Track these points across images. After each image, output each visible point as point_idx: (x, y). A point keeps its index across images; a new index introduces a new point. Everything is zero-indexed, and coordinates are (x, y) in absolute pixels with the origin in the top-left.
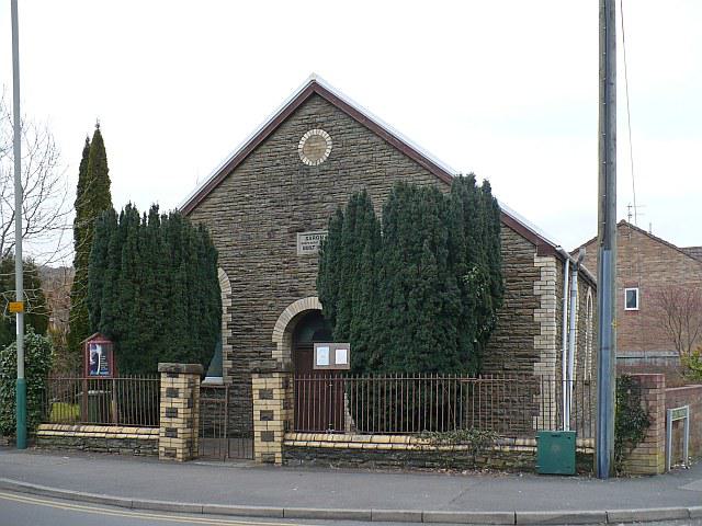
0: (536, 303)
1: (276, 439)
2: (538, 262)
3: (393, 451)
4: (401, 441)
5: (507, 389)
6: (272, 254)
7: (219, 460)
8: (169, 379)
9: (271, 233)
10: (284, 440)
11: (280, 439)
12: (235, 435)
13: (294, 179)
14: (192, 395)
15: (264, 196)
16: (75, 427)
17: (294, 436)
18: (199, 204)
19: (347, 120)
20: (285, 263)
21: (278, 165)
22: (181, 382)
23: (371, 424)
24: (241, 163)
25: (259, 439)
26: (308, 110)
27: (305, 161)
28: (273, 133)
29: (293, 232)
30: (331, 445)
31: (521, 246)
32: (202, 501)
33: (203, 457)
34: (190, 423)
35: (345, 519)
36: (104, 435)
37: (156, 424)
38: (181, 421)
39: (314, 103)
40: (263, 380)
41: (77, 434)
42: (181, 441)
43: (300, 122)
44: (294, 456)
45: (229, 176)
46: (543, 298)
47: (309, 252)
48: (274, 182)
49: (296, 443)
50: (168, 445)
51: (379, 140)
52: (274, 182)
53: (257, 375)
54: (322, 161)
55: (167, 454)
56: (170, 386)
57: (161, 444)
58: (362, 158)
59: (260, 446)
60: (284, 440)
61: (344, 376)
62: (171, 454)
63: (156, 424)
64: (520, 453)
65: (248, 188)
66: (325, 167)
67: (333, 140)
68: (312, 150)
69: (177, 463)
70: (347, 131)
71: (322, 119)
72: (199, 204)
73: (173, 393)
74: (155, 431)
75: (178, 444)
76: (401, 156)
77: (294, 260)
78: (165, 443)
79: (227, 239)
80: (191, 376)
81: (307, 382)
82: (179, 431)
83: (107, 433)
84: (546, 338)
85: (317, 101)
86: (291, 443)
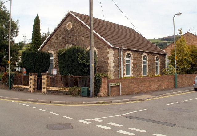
0: (108, 59)
2: (109, 50)
9: (62, 45)
10: (47, 89)
13: (66, 33)
14: (35, 79)
24: (57, 30)
29: (65, 44)
35: (78, 104)
37: (28, 85)
39: (69, 16)
44: (52, 92)
45: (55, 33)
48: (62, 34)
52: (62, 34)
58: (77, 28)
59: (43, 90)
63: (28, 85)
68: (69, 27)
73: (31, 79)
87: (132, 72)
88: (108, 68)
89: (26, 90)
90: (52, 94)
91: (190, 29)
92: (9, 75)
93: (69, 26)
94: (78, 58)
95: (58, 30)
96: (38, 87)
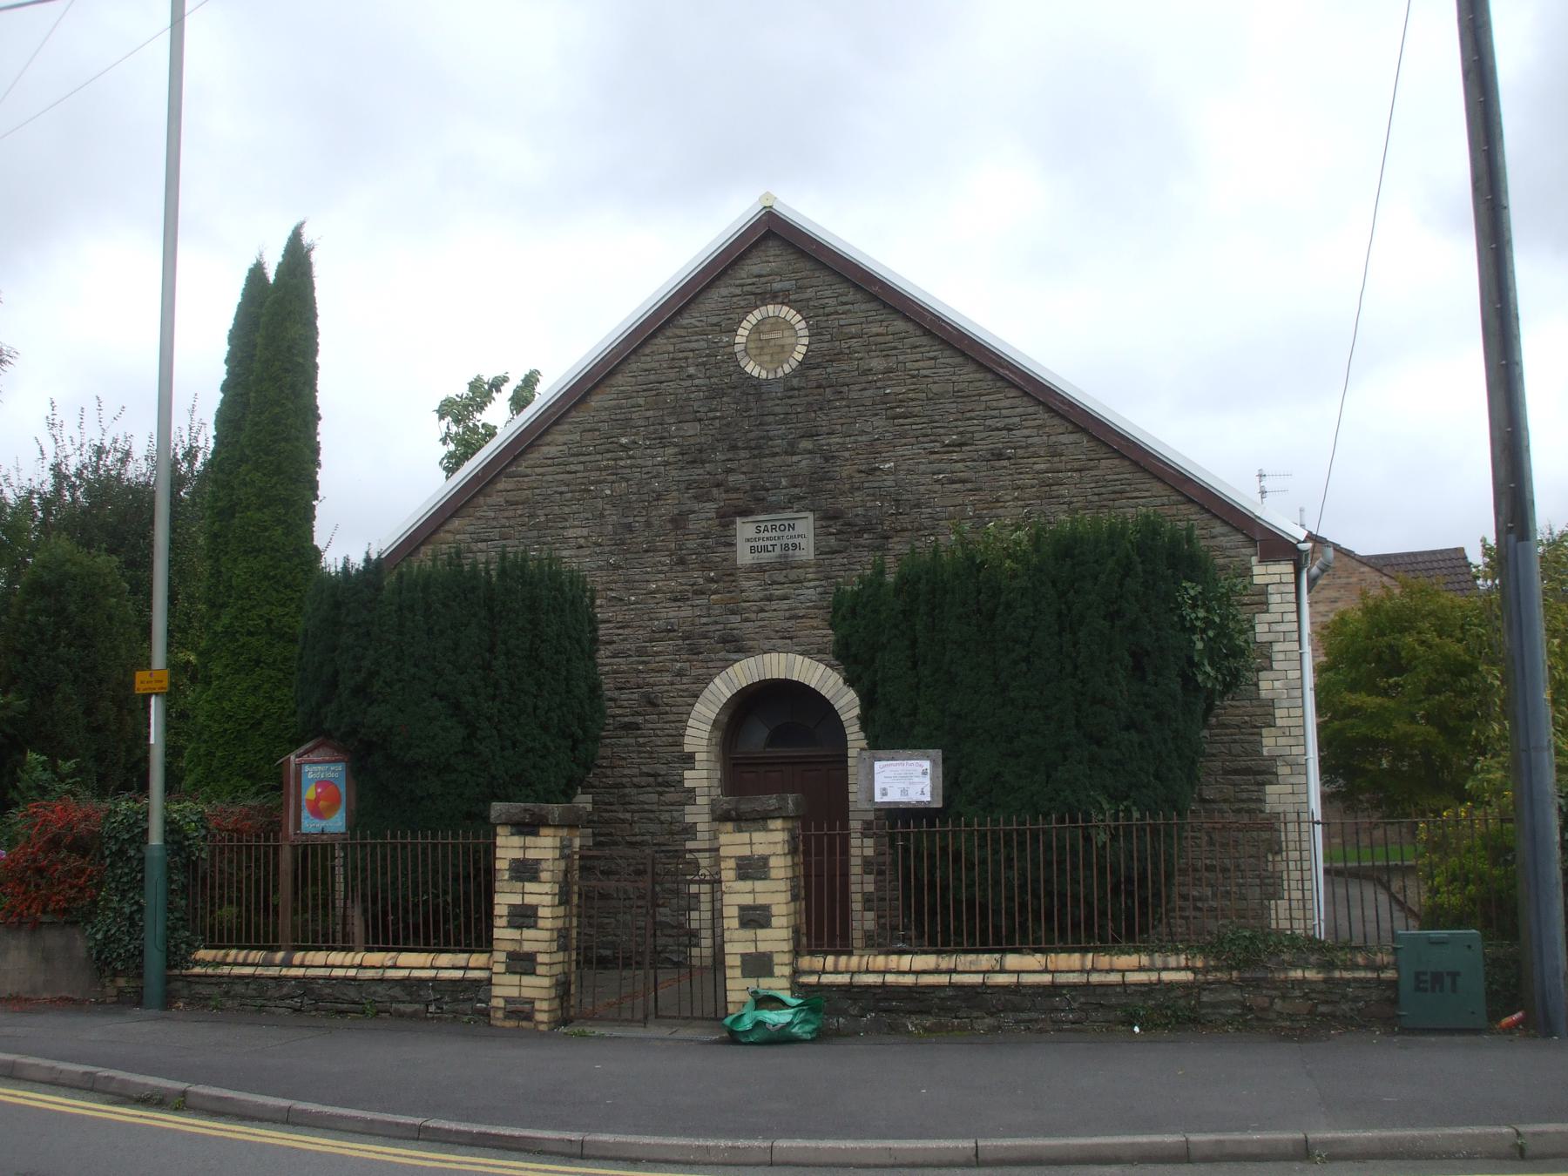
1: (777, 970)
3: (1054, 989)
4: (1069, 966)
5: (1211, 843)
6: (682, 562)
7: (631, 1021)
8: (517, 840)
11: (787, 971)
12: (603, 963)
15: (663, 442)
16: (280, 955)
17: (817, 962)
18: (516, 458)
19: (841, 288)
20: (712, 580)
21: (690, 377)
22: (544, 847)
23: (997, 928)
25: (738, 972)
26: (754, 266)
27: (752, 368)
28: (680, 312)
29: (726, 518)
30: (909, 980)
31: (1222, 541)
32: (766, 1133)
33: (593, 1018)
34: (562, 939)
36: (352, 973)
37: (484, 943)
38: (546, 935)
39: (772, 237)
40: (745, 837)
41: (285, 972)
42: (546, 982)
43: (738, 291)
44: (839, 1014)
46: (1276, 647)
47: (765, 557)
49: (826, 979)
50: (514, 992)
51: (910, 327)
53: (729, 826)
54: (787, 369)
55: (510, 1014)
56: (518, 854)
57: (496, 991)
60: (796, 972)
61: (931, 824)
62: (520, 1011)
63: (484, 943)
64: (1348, 982)
65: (626, 424)
66: (795, 382)
67: (808, 327)
69: (536, 1034)
70: (841, 309)
71: (787, 285)
72: (516, 458)
73: (525, 871)
74: (478, 959)
75: (537, 987)
76: (959, 360)
77: (730, 573)
78: (507, 987)
79: (579, 532)
80: (564, 832)
81: (435, 846)
82: (540, 958)
83: (360, 966)
84: (1286, 732)
85: (773, 249)
86: (813, 979)
87: (692, 778)
88: (1270, 743)
89: (461, 1006)
90: (894, 1029)
91: (1266, 483)
92: (156, 838)
93: (773, 341)
94: (1193, 629)
95: (619, 379)
96: (635, 948)
